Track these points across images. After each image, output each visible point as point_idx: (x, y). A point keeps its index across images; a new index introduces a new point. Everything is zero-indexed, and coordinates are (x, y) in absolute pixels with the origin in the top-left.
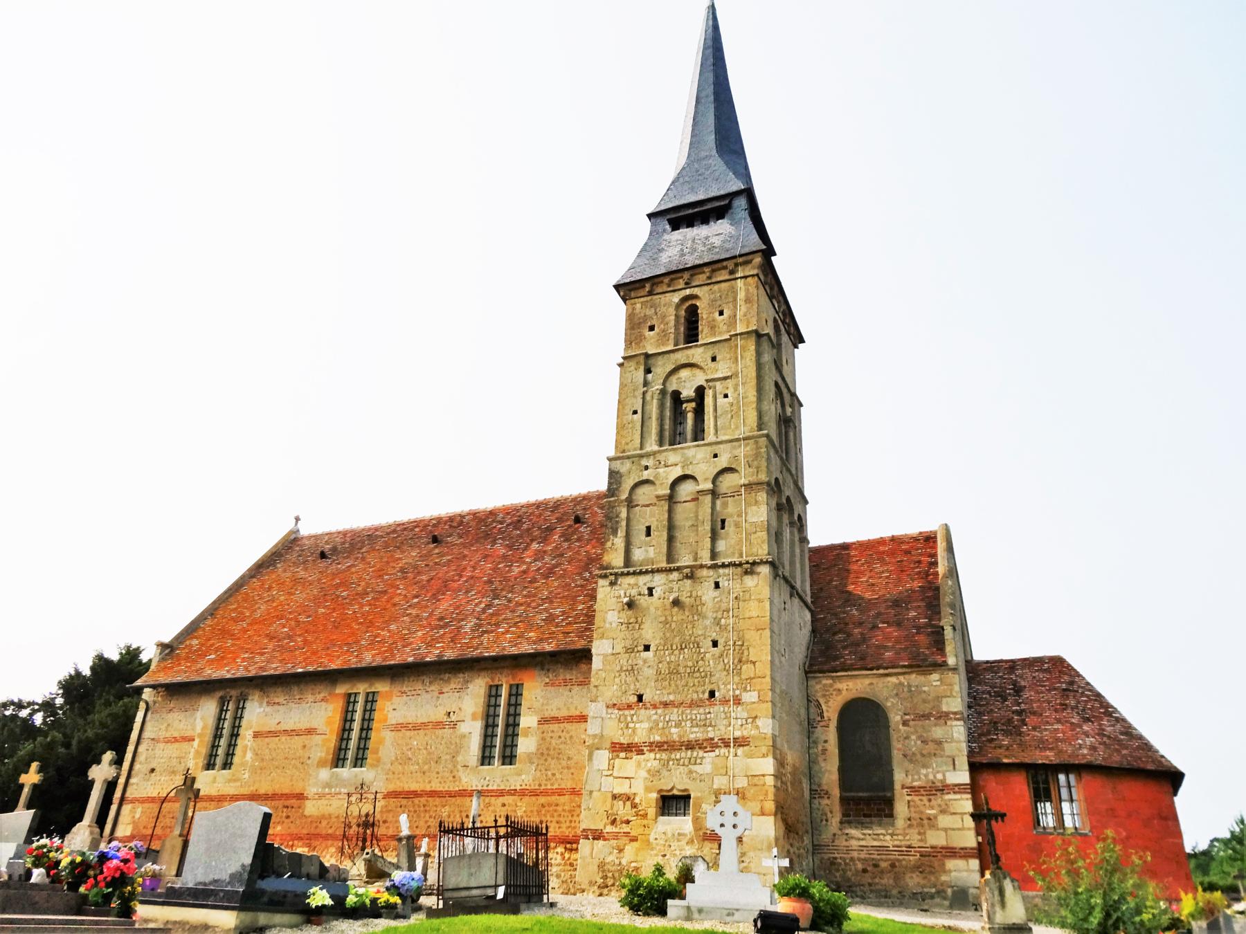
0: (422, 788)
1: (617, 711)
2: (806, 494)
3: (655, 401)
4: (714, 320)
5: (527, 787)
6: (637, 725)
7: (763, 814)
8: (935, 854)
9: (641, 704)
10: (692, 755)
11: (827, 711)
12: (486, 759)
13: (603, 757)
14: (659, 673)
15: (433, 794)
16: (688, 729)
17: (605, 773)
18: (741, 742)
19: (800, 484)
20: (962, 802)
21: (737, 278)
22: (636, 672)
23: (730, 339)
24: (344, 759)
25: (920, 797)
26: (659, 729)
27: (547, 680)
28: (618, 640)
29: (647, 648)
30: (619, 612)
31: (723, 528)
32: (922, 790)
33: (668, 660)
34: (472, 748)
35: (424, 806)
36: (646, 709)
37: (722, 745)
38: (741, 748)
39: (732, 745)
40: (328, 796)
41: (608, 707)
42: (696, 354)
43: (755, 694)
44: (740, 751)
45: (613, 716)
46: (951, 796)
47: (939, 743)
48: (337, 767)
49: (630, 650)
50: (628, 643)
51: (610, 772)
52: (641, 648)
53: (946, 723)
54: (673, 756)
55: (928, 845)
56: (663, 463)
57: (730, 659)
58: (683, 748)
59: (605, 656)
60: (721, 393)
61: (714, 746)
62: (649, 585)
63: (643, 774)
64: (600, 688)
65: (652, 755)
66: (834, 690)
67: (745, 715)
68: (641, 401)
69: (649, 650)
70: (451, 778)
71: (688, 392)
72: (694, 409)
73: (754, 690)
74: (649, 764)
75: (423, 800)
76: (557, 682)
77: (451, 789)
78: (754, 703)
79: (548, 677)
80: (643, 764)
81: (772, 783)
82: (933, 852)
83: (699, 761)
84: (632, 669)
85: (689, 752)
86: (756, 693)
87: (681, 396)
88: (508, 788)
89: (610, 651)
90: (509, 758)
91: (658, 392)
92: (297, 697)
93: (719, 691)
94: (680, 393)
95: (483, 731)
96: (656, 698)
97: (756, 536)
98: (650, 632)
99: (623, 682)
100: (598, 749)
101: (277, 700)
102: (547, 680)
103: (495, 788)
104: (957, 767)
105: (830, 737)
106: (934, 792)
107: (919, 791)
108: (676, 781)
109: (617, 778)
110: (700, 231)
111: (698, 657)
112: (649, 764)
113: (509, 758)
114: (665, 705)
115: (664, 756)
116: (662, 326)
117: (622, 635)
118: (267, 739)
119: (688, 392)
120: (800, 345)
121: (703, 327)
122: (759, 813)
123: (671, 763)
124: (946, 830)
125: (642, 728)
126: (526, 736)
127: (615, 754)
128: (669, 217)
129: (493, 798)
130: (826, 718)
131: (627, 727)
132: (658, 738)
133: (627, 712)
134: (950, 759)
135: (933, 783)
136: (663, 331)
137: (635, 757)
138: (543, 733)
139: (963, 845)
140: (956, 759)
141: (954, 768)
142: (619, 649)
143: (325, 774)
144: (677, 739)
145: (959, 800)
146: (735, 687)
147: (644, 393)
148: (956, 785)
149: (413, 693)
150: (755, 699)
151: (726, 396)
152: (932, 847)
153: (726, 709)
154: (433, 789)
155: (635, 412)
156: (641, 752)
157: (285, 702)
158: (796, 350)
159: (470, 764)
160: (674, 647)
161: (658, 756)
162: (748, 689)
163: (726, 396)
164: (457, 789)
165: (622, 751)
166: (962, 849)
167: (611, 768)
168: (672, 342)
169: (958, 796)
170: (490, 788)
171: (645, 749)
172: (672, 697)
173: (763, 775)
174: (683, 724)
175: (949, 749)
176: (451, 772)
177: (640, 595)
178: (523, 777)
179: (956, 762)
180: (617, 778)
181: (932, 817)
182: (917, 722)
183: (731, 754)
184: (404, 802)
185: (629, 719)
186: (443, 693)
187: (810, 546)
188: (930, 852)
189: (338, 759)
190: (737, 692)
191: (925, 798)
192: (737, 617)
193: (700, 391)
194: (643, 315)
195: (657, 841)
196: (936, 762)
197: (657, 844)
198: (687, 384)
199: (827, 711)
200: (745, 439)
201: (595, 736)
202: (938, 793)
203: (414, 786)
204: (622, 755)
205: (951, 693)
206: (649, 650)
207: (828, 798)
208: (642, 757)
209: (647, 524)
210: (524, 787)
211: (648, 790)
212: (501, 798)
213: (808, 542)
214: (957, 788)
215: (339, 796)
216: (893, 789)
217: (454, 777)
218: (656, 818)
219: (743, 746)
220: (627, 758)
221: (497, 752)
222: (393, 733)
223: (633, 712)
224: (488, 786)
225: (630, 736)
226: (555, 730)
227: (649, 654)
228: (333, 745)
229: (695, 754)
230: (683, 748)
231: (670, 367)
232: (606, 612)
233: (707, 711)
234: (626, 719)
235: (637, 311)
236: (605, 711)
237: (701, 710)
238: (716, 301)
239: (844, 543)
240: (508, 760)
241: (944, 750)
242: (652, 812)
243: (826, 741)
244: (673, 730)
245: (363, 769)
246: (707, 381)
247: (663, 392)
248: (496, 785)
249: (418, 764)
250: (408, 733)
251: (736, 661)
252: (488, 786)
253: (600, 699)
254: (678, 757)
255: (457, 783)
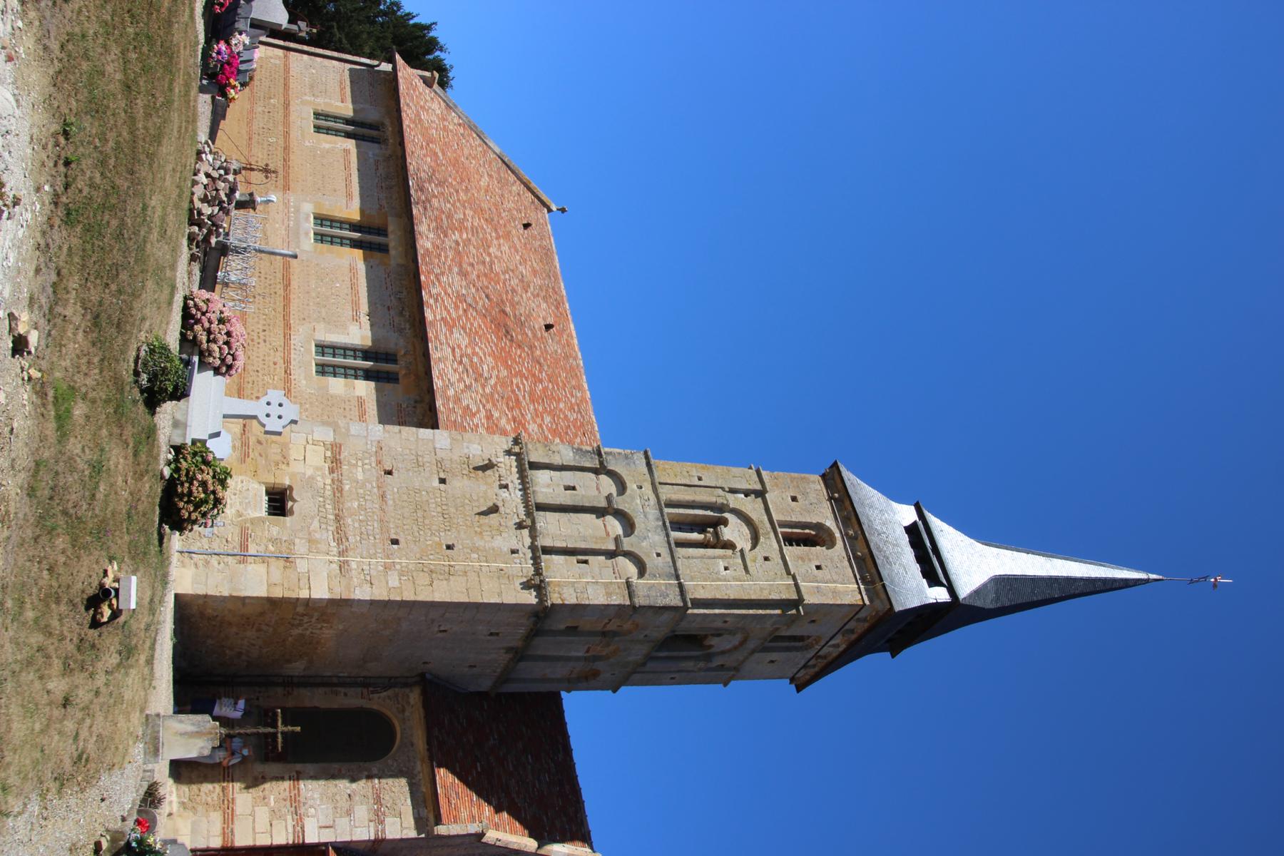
0: (292, 290)
1: (374, 449)
2: (623, 689)
3: (713, 499)
4: (810, 560)
5: (293, 385)
6: (360, 469)
7: (269, 585)
8: (226, 802)
9: (383, 473)
10: (330, 520)
11: (379, 698)
12: (322, 348)
13: (328, 435)
14: (419, 491)
15: (287, 300)
16: (357, 518)
17: (310, 437)
18: (343, 566)
19: (637, 677)
20: (284, 833)
21: (858, 584)
22: (416, 469)
23: (788, 573)
24: (322, 225)
25: (288, 790)
26: (356, 489)
27: (404, 406)
28: (450, 454)
29: (443, 481)
30: (481, 456)
31: (578, 562)
32: (296, 792)
33: (430, 501)
34: (333, 335)
35: (276, 293)
36: (377, 478)
37: (341, 550)
38: (338, 568)
39: (341, 559)
40: (286, 211)
41: (379, 442)
42: (769, 544)
43: (396, 584)
44: (335, 567)
45: (369, 447)
46: (290, 823)
47: (349, 813)
48: (315, 218)
49: (439, 463)
50: (447, 464)
51: (311, 442)
52: (442, 476)
53: (371, 821)
54: (328, 501)
55: (236, 795)
56: (647, 503)
57: (432, 562)
58: (337, 511)
59: (433, 441)
60: (728, 563)
61: (339, 542)
62: (510, 486)
63: (309, 472)
64: (398, 435)
65: (329, 481)
66: (403, 706)
67: (373, 573)
68: (714, 485)
69: (440, 483)
70: (302, 316)
71: (727, 533)
72: (709, 541)
73: (401, 583)
74: (319, 478)
75: (281, 292)
76: (403, 415)
77: (292, 317)
78: (387, 583)
79: (407, 407)
80: (320, 473)
81: (301, 596)
82: (228, 800)
83: (323, 526)
84: (419, 466)
85: (332, 517)
86: (399, 585)
87: (722, 527)
88: (292, 367)
89: (438, 446)
90: (323, 370)
91: (725, 502)
92: (383, 185)
93: (399, 548)
94: (726, 526)
95: (350, 346)
96: (390, 488)
97: (572, 592)
98: (460, 484)
99: (405, 457)
100: (334, 431)
101: (381, 168)
102: (404, 406)
103: (292, 356)
104: (323, 830)
105: (351, 700)
106: (294, 805)
107: (294, 789)
108: (301, 504)
109: (305, 448)
110: (909, 555)
111: (436, 531)
112: (319, 478)
113: (323, 370)
114: (383, 497)
115: (328, 493)
116: (798, 509)
117: (456, 457)
118: (342, 160)
119: (727, 533)
120: (793, 686)
121: (802, 550)
122: (269, 582)
123: (321, 499)
124: (253, 815)
125: (359, 473)
126: (346, 385)
127: (330, 446)
128: (920, 523)
129: (282, 355)
130: (371, 696)
131: (357, 459)
132: (347, 487)
133: (373, 459)
134: (331, 823)
135: (304, 804)
136: (793, 511)
137: (327, 465)
138: (349, 401)
139: (236, 832)
140: (332, 830)
141: (321, 827)
142: (440, 454)
143: (308, 209)
144: (346, 506)
145: (287, 830)
146: (404, 564)
147: (722, 488)
148: (303, 828)
149: (389, 284)
150: (391, 584)
151: (726, 569)
152: (233, 799)
153: (380, 555)
154: (292, 300)
155: (700, 479)
156: (332, 471)
157: (378, 174)
158: (788, 681)
159: (316, 333)
160: (444, 507)
161: (328, 487)
162: (402, 578)
163: (726, 569)
164: (292, 322)
165: (332, 453)
166: (232, 831)
167: (315, 443)
168: (782, 518)
169: (290, 830)
170: (292, 351)
171: (335, 475)
172: (390, 502)
173: (310, 588)
174: (362, 513)
175: (343, 823)
176: (309, 317)
177: (500, 476)
178: (304, 382)
179: (328, 830)
180: (305, 448)
181: (266, 800)
182: (371, 791)
183: (331, 558)
184: (279, 275)
185: (367, 461)
186: (389, 310)
187: (563, 694)
188: (228, 796)
189: (322, 220)
190: (398, 567)
191: (287, 793)
192: (481, 569)
193: (729, 545)
194: (808, 491)
195: (239, 483)
196: (327, 808)
197: (237, 482)
198: (734, 531)
199: (379, 698)
200: (681, 586)
201: (348, 430)
202: (293, 809)
203: (294, 284)
204: (329, 454)
205: (406, 828)
206: (440, 483)
207: (284, 695)
208: (327, 472)
209: (577, 487)
210: (293, 382)
211: (293, 476)
212: (282, 361)
213: (568, 691)
214: (300, 826)
215: (286, 220)
216: (295, 762)
217: (304, 319)
218: (263, 483)
219: (341, 570)
220: (325, 458)
221: (329, 359)
222: (348, 266)
223: (374, 465)
224: (295, 349)
225: (349, 462)
226: (352, 412)
227: (436, 483)
228: (337, 215)
229: (331, 523)
230: (337, 511)
231: (754, 516)
232: (479, 444)
233: (377, 537)
234: (367, 459)
235: (812, 486)
236: (373, 439)
237: (377, 531)
238: (832, 562)
239: (569, 737)
240: (320, 369)
241: (341, 817)
242: (271, 480)
243: (346, 694)
244: (356, 504)
245: (312, 241)
246: (742, 551)
247: (722, 508)
248: (295, 356)
249: (317, 288)
250: (347, 279)
251: (432, 567)
252: (295, 349)
253: (387, 435)
254: (327, 506)
255: (297, 322)
